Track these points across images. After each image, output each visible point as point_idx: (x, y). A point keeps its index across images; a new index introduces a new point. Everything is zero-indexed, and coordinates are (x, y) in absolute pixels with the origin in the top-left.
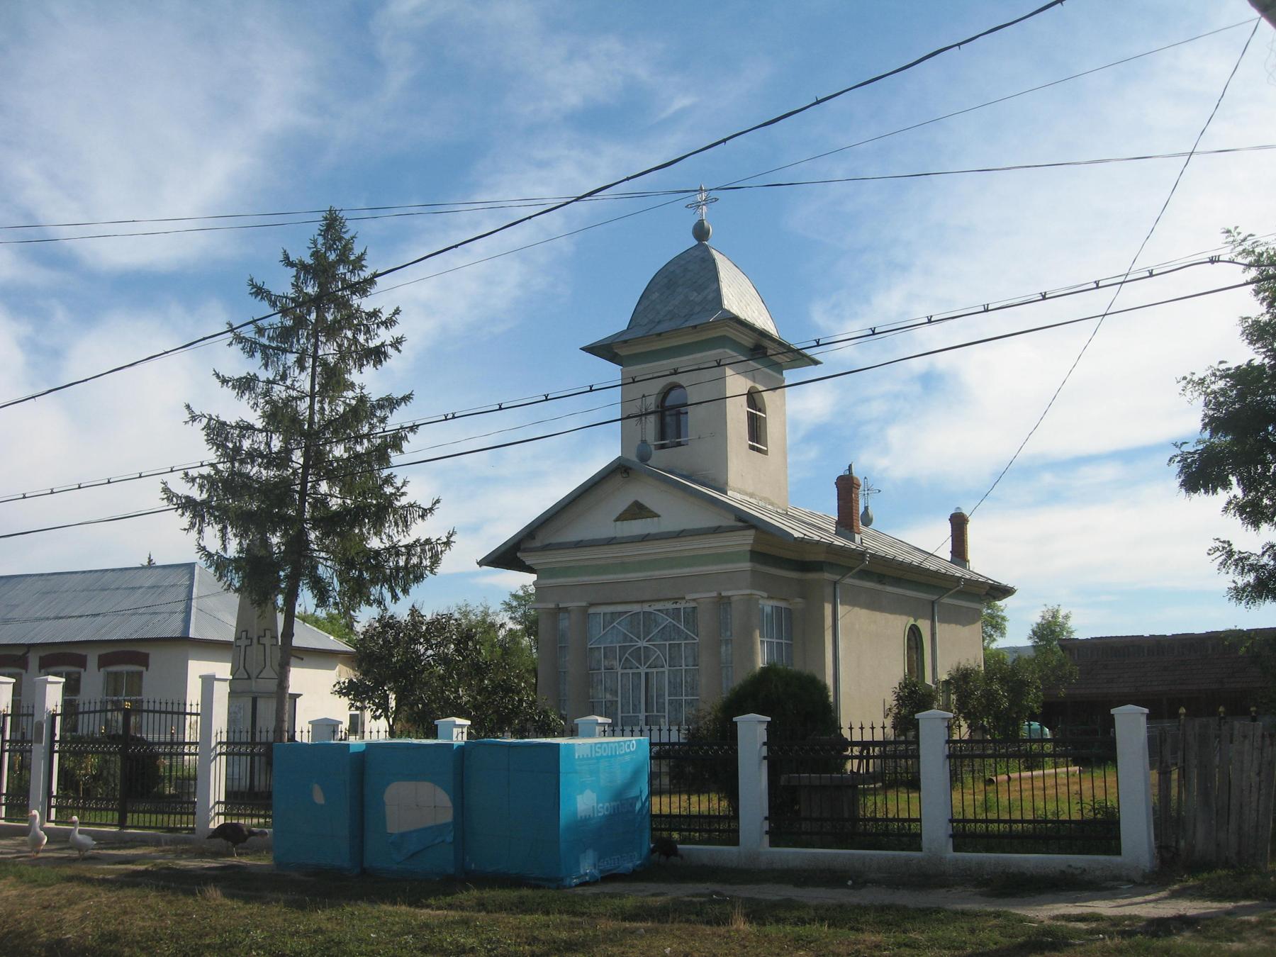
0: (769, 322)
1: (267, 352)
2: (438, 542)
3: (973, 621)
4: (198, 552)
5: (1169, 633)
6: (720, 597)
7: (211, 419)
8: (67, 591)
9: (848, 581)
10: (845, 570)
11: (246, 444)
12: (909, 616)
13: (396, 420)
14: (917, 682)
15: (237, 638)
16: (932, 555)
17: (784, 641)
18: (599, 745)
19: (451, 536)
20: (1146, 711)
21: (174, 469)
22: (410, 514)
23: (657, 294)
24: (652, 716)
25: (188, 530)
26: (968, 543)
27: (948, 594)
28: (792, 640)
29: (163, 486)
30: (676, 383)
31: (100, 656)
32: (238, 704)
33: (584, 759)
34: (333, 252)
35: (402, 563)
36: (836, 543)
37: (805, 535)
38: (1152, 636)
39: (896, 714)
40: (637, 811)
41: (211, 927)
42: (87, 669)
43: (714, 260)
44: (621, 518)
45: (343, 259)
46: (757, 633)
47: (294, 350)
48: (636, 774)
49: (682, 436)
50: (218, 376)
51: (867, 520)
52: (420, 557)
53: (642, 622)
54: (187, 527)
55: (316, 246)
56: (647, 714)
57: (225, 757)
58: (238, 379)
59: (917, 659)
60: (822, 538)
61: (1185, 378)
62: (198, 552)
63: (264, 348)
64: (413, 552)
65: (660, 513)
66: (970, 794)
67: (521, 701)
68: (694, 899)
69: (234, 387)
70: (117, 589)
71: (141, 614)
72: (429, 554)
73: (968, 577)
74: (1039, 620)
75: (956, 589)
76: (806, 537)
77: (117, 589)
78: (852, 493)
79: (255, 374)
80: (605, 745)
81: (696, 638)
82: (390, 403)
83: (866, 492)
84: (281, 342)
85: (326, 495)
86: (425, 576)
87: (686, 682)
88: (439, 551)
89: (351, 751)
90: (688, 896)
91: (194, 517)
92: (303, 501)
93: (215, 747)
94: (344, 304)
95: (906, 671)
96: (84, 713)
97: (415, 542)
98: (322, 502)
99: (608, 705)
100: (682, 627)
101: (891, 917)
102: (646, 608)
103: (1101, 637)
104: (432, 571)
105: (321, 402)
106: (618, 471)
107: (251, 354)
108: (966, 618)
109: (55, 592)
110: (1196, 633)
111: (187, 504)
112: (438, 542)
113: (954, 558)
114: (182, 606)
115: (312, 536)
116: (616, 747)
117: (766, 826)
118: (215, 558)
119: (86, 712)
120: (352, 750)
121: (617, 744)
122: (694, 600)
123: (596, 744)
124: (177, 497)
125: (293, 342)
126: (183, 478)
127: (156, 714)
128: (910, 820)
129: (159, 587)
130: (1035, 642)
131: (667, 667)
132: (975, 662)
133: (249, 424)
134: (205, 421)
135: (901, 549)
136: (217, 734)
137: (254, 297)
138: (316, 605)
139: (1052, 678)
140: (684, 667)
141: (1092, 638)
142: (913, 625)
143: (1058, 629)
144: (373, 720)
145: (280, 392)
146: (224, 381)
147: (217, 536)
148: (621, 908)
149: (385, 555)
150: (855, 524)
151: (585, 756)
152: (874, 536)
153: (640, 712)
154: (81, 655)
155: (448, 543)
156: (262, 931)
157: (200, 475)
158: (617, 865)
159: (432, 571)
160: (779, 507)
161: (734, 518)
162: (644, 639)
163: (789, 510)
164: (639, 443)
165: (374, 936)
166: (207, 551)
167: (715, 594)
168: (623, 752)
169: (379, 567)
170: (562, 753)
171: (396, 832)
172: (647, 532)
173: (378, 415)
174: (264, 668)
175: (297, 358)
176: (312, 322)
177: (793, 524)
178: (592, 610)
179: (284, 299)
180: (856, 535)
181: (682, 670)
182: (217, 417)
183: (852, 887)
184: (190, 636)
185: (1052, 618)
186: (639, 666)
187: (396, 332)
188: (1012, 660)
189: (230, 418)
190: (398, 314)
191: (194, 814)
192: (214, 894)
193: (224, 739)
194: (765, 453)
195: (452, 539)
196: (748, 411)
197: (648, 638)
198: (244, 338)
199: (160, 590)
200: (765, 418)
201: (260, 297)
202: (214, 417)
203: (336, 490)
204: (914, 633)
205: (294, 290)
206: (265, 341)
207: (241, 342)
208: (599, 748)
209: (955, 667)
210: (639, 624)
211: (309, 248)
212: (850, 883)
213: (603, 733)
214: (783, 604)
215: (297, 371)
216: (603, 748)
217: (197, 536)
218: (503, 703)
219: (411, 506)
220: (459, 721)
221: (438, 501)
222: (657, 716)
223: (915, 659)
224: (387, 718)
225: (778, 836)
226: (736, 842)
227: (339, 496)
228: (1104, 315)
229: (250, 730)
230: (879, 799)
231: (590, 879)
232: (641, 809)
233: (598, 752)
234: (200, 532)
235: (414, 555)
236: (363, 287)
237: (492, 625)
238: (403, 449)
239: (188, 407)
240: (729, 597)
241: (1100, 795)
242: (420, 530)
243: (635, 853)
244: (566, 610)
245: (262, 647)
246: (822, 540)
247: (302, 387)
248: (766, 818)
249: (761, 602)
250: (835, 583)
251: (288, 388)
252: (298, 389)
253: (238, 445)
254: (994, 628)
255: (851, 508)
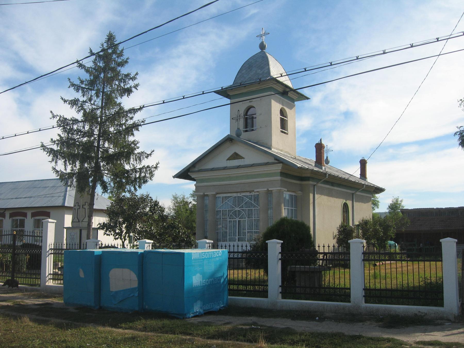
0: (289, 82)
1: (84, 90)
2: (152, 167)
3: (368, 202)
4: (52, 170)
5: (444, 207)
6: (268, 190)
7: (61, 117)
8: (21, 188)
9: (320, 185)
10: (318, 180)
11: (75, 127)
12: (343, 199)
13: (137, 117)
14: (346, 225)
15: (74, 206)
16: (352, 175)
17: (293, 208)
18: (204, 253)
19: (157, 165)
20: (456, 240)
21: (29, 132)
22: (142, 156)
23: (245, 71)
24: (241, 238)
25: (51, 162)
26: (367, 171)
27: (359, 191)
28: (297, 208)
29: (42, 144)
30: (252, 106)
31: (32, 213)
32: (74, 232)
33: (196, 260)
34: (110, 49)
35: (138, 176)
36: (315, 169)
37: (302, 166)
38: (437, 209)
39: (338, 238)
40: (221, 283)
41: (18, 337)
42: (6, 219)
43: (267, 57)
44: (229, 159)
45: (114, 52)
46: (283, 205)
47: (95, 89)
48: (221, 266)
49: (254, 127)
50: (62, 99)
51: (327, 162)
52: (145, 173)
53: (237, 200)
54: (51, 161)
55: (103, 47)
56: (239, 237)
57: (53, 255)
58: (71, 100)
59: (346, 216)
60: (309, 167)
61: (461, 100)
62: (52, 170)
63: (83, 88)
64: (142, 171)
65: (244, 157)
66: (367, 270)
67: (179, 232)
68: (244, 327)
69: (69, 104)
70: (40, 187)
71: (48, 197)
72: (149, 172)
73: (367, 184)
74: (391, 202)
75: (362, 189)
76: (302, 167)
77: (40, 187)
78: (321, 150)
79: (78, 99)
80: (207, 253)
81: (258, 207)
82: (134, 111)
83: (327, 151)
84: (90, 86)
85: (107, 148)
86: (148, 181)
87: (254, 224)
88: (153, 171)
89: (95, 255)
90: (241, 325)
91: (54, 156)
92: (98, 150)
93: (49, 251)
94: (113, 70)
95: (342, 221)
96: (4, 235)
97: (143, 167)
98: (106, 151)
99: (224, 233)
100: (253, 203)
101: (337, 341)
102: (239, 195)
103: (417, 209)
104: (151, 179)
105: (105, 110)
106: (228, 140)
107: (77, 90)
108: (366, 200)
109: (16, 189)
110: (454, 207)
111: (51, 151)
112: (152, 167)
113: (361, 177)
114: (63, 194)
115: (102, 164)
116: (212, 254)
117: (280, 290)
118: (60, 173)
119: (5, 235)
120: (95, 254)
121: (212, 253)
122: (258, 192)
123: (202, 253)
124: (47, 148)
125: (95, 86)
126: (50, 141)
127: (28, 237)
128: (345, 288)
129: (55, 187)
130: (389, 210)
131: (247, 218)
132: (369, 217)
133: (76, 119)
134: (58, 118)
135: (340, 173)
136: (50, 245)
137: (78, 68)
138: (102, 192)
139: (399, 224)
140: (253, 218)
141: (414, 209)
142: (345, 203)
143: (398, 206)
144: (115, 240)
145: (88, 106)
146: (65, 101)
147: (63, 164)
148: (208, 332)
149: (131, 172)
150: (322, 162)
151: (197, 258)
152: (330, 168)
153: (236, 236)
154: (25, 213)
155: (156, 168)
156: (40, 340)
157: (57, 140)
158: (212, 307)
159: (151, 179)
160: (292, 156)
161: (274, 159)
162: (238, 207)
163: (296, 157)
164: (237, 129)
165: (89, 345)
166: (56, 170)
167: (266, 189)
168: (215, 256)
169: (128, 178)
170: (186, 257)
171: (114, 291)
172: (239, 165)
173: (129, 116)
174: (85, 218)
175: (96, 92)
176: (102, 78)
177: (298, 162)
178: (218, 196)
179: (91, 69)
180: (323, 167)
181: (253, 219)
182: (63, 116)
183: (318, 321)
184: (65, 205)
185: (396, 201)
186: (236, 218)
187: (136, 82)
188: (384, 217)
189: (69, 117)
190: (137, 75)
191: (40, 278)
192: (26, 320)
193: (53, 248)
194: (287, 134)
195: (158, 166)
196: (280, 117)
197: (239, 207)
198: (74, 84)
199: (55, 188)
200: (287, 120)
201: (81, 68)
202: (62, 116)
203: (112, 146)
204: (345, 206)
205: (94, 64)
206: (84, 86)
207: (73, 86)
208: (203, 254)
209: (361, 220)
210: (236, 201)
211: (100, 47)
212: (317, 318)
213: (209, 247)
214: (293, 194)
215: (95, 98)
216: (205, 254)
217: (55, 164)
218: (171, 233)
219: (142, 153)
220: (148, 241)
221: (153, 151)
222: (243, 238)
223: (346, 216)
224: (121, 239)
225: (285, 294)
226: (267, 297)
227: (112, 148)
228: (440, 55)
229: (79, 244)
230: (332, 272)
231: (199, 314)
232: (224, 282)
233: (203, 257)
234: (56, 162)
235: (142, 172)
236: (122, 64)
237: (187, 202)
238: (139, 130)
239: (51, 112)
240: (271, 191)
241: (428, 275)
242: (146, 162)
243: (221, 302)
244: (207, 195)
245: (84, 209)
246: (309, 168)
247: (98, 104)
248: (280, 286)
249: (285, 192)
250: (314, 185)
251: (92, 104)
252: (97, 105)
253: (72, 127)
254: (374, 205)
255: (321, 156)
